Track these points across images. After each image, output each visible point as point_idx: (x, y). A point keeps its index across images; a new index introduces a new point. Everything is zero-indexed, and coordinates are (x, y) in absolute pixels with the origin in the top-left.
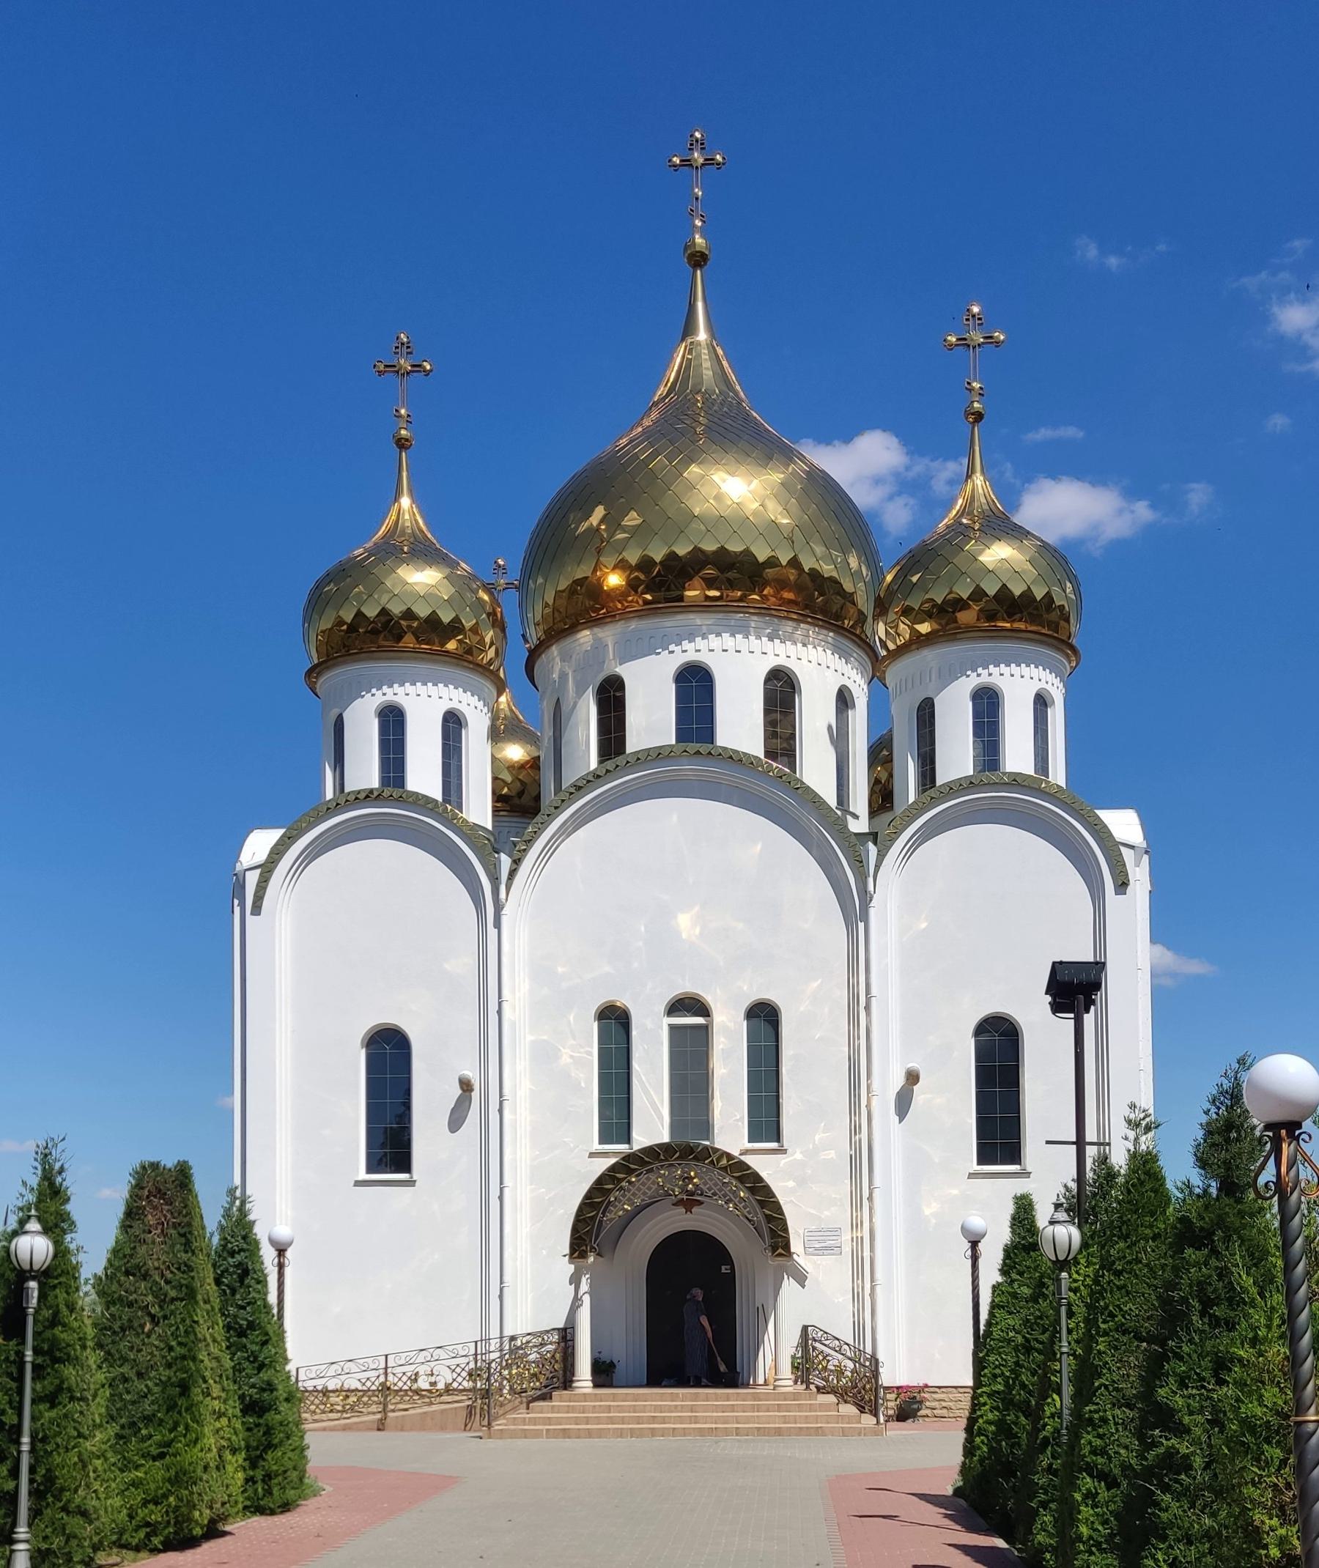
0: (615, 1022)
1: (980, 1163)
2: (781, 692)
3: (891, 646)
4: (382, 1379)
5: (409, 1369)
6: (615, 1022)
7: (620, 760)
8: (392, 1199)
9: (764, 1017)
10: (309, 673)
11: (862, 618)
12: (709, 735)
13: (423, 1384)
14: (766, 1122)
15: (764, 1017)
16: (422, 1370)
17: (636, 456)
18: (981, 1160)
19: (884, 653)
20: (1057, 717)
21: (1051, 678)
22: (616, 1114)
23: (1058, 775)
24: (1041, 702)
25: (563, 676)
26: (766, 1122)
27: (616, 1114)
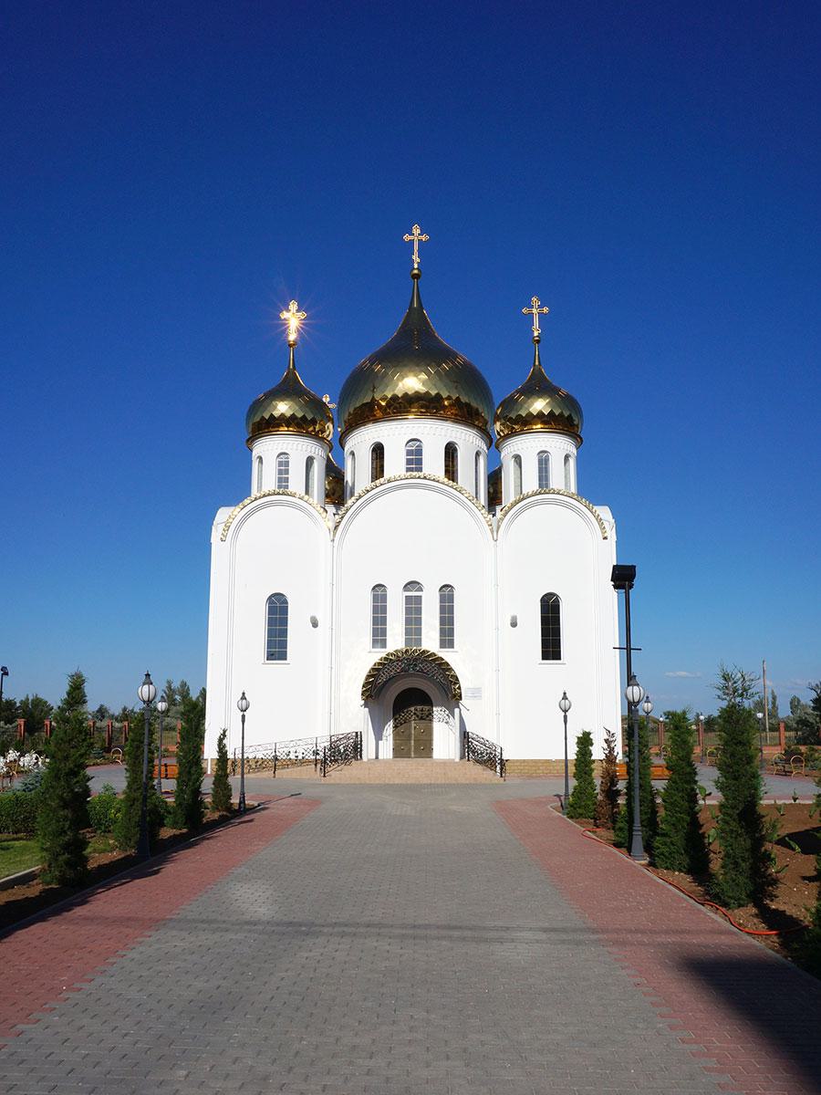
0: (379, 593)
1: (543, 659)
2: (451, 451)
3: (502, 434)
4: (274, 754)
5: (286, 750)
6: (379, 593)
7: (382, 480)
8: (276, 665)
9: (447, 594)
10: (248, 440)
11: (486, 423)
12: (547, 486)
13: (292, 756)
14: (447, 639)
15: (447, 594)
16: (292, 750)
17: (373, 370)
18: (543, 659)
19: (498, 437)
20: (572, 462)
21: (575, 451)
22: (379, 636)
23: (573, 489)
24: (310, 461)
25: (498, 408)
26: (447, 639)
27: (379, 636)
